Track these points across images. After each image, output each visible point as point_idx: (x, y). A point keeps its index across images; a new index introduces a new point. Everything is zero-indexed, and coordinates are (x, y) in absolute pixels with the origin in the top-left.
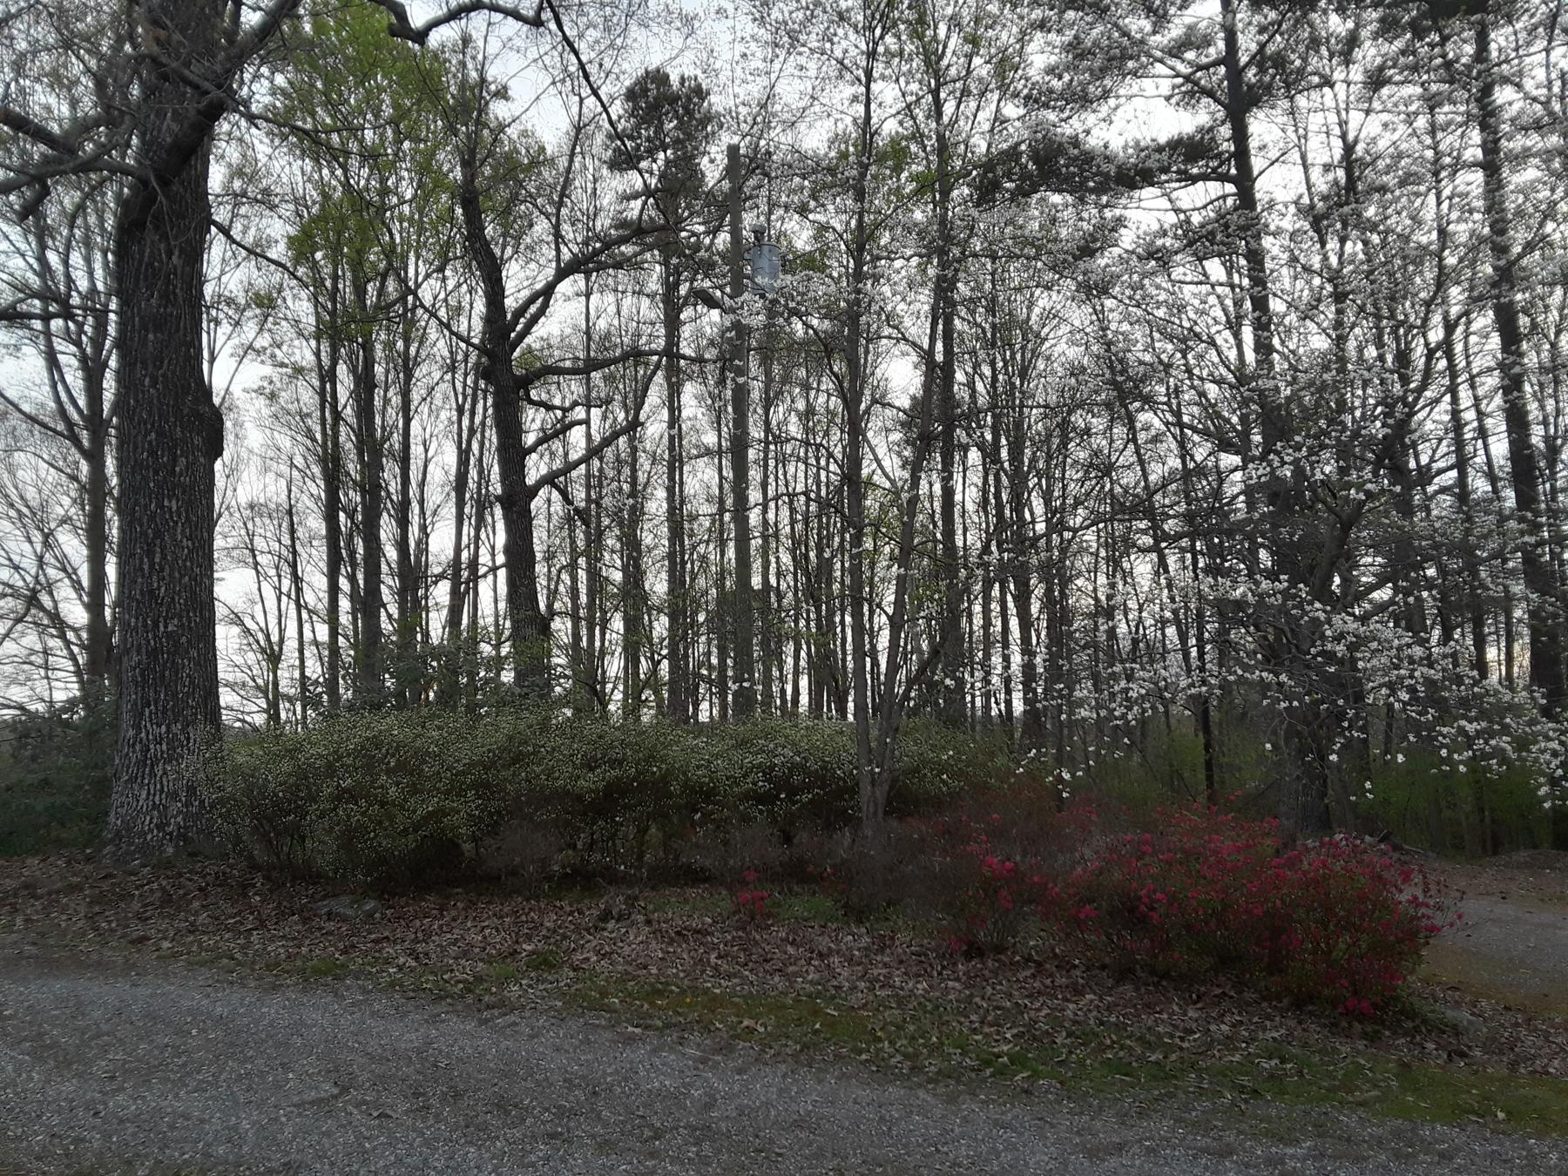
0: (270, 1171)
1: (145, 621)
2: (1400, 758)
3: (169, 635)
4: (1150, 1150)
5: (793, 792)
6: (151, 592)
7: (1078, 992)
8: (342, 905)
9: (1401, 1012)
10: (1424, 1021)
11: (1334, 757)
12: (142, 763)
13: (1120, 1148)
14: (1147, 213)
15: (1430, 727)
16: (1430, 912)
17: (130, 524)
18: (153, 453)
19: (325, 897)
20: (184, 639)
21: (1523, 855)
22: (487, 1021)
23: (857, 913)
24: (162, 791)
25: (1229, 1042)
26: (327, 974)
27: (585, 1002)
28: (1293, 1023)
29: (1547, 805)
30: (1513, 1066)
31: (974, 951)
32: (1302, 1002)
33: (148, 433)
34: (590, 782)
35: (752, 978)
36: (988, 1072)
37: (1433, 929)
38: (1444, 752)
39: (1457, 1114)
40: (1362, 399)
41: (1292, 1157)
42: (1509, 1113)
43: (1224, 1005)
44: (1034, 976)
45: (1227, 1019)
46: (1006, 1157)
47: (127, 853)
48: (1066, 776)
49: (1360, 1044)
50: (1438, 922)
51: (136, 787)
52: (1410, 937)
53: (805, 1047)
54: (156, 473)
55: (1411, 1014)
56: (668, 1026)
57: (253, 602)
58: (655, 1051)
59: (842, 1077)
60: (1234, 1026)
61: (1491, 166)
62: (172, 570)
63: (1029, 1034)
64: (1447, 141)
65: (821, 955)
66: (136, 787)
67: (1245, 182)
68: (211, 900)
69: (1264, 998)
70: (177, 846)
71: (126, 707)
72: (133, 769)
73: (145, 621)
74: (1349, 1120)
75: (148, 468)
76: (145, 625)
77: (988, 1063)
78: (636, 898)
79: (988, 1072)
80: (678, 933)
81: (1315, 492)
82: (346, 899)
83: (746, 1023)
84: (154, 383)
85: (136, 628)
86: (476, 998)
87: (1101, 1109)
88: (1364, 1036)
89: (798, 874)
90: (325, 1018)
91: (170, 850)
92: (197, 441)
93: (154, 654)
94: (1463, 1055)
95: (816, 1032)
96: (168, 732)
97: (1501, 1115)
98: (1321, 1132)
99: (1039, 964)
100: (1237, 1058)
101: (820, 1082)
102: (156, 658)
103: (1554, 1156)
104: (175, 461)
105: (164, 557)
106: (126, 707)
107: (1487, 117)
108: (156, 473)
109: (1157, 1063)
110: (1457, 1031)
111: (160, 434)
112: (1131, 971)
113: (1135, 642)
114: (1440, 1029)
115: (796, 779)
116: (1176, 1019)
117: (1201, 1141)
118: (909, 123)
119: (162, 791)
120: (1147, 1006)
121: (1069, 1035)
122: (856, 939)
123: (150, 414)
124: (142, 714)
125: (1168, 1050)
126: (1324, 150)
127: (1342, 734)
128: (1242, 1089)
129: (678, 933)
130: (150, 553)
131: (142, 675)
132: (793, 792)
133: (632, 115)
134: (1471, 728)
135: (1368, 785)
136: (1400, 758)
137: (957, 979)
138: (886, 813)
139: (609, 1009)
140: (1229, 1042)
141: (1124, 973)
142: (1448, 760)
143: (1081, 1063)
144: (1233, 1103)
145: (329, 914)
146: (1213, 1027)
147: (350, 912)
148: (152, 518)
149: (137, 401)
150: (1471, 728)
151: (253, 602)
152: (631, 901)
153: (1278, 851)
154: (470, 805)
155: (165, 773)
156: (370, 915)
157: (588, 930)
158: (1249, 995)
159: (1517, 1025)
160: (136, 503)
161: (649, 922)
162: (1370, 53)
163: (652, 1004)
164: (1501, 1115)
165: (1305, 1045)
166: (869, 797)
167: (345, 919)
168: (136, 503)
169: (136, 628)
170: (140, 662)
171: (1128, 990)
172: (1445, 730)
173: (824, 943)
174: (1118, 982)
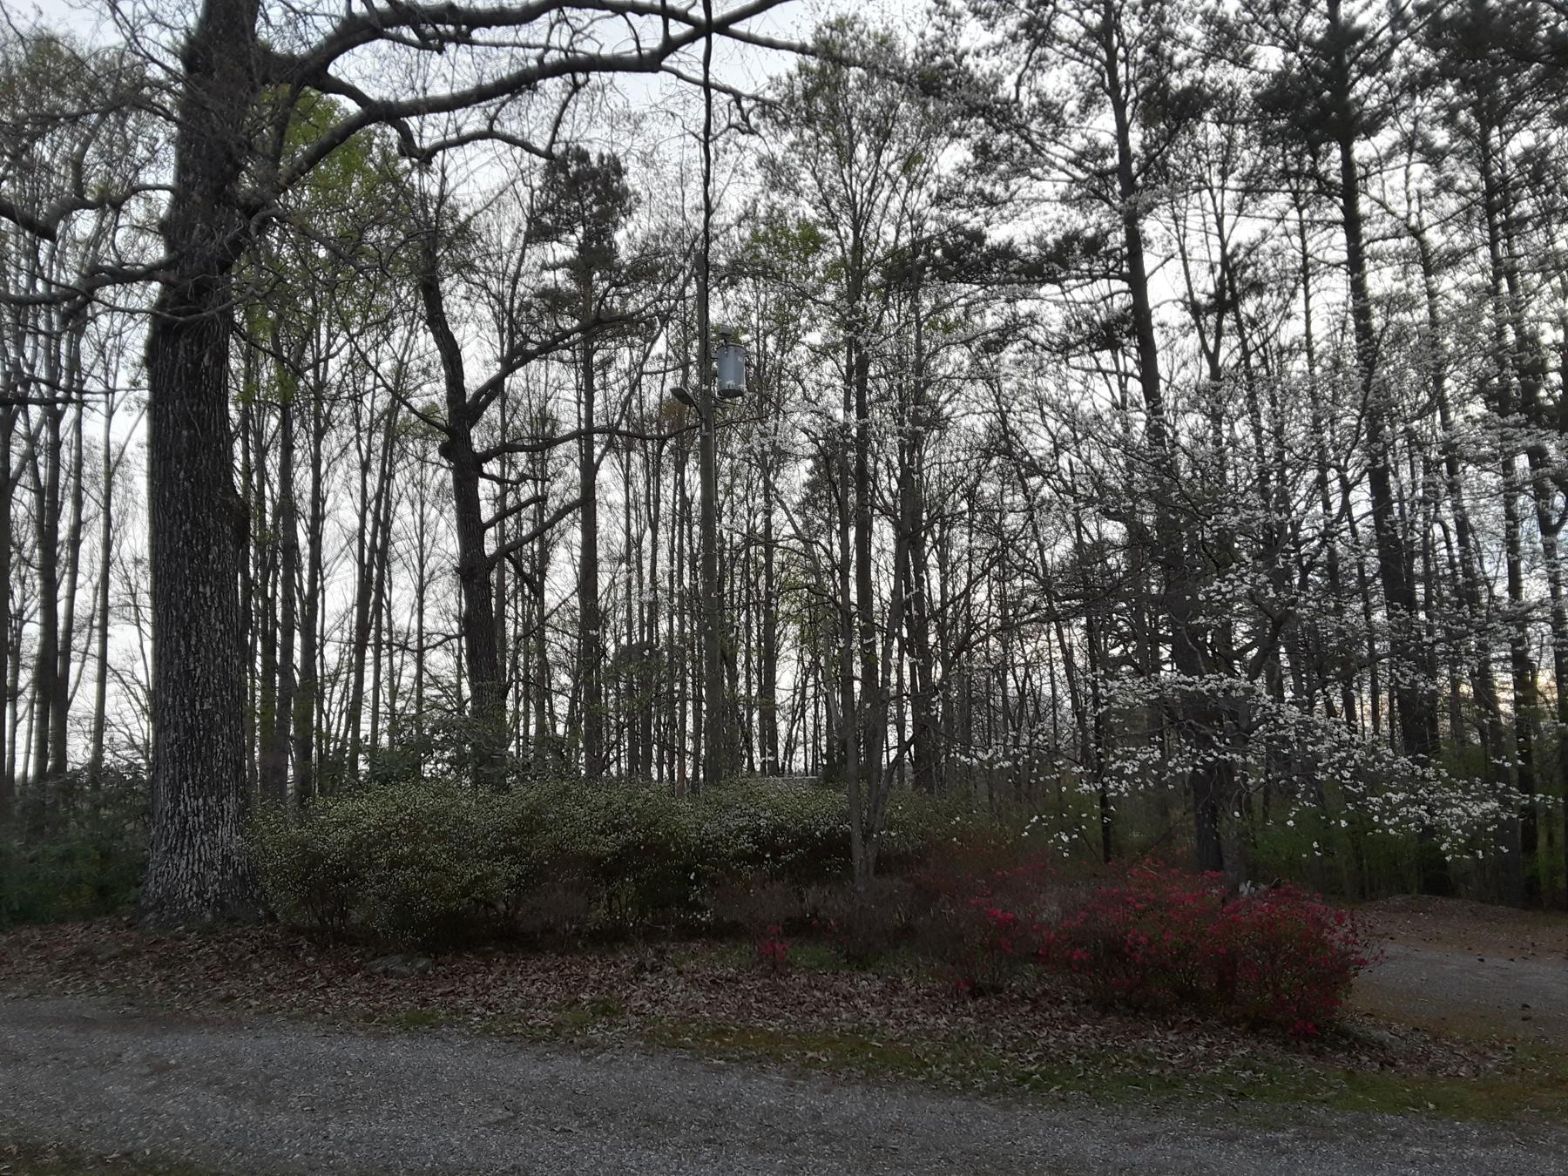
0: (504, 1172)
1: (182, 700)
2: (1343, 823)
3: (205, 713)
4: (1175, 1139)
5: (777, 852)
6: (188, 672)
7: (1075, 1024)
8: (395, 962)
9: (1336, 1032)
10: (1357, 1039)
11: (1290, 823)
12: (181, 834)
13: (1152, 1138)
14: (1051, 308)
15: (1363, 796)
16: (1356, 948)
17: (167, 608)
18: (188, 543)
19: (375, 957)
20: (218, 717)
21: (1398, 900)
22: (590, 1057)
23: (859, 961)
24: (200, 860)
25: (1208, 1059)
26: (418, 1024)
27: (658, 1041)
28: (1254, 1043)
29: (1448, 859)
30: (1432, 1071)
31: (976, 992)
32: (1256, 1025)
33: (183, 523)
34: (607, 845)
35: (794, 1018)
36: (1027, 1086)
37: (1363, 963)
38: (1376, 818)
39: (1399, 1107)
40: (1240, 474)
41: (1284, 1139)
42: (1437, 1104)
43: (1196, 1030)
44: (1032, 1011)
45: (1201, 1041)
46: (1067, 1147)
47: (170, 919)
48: (1066, 839)
49: (1310, 1058)
50: (1365, 955)
51: (175, 857)
52: (1337, 973)
53: (868, 1071)
54: (191, 561)
55: (1345, 1034)
56: (745, 1058)
57: (133, 659)
58: (745, 1078)
59: (909, 1094)
60: (1207, 1046)
61: (1355, 263)
62: (207, 651)
63: (1045, 1056)
64: (1316, 239)
65: (845, 997)
66: (175, 857)
67: (1137, 283)
68: (266, 961)
69: (1225, 1024)
70: (214, 913)
71: (162, 783)
72: (172, 841)
73: (182, 700)
74: (1319, 1113)
75: (183, 556)
76: (182, 704)
77: (1025, 1081)
78: (664, 952)
79: (1027, 1086)
80: (713, 982)
81: (1178, 544)
82: (398, 958)
83: (810, 1054)
84: (187, 479)
85: (174, 706)
86: (556, 1038)
87: (1127, 1112)
88: (1311, 1051)
89: (803, 928)
90: (446, 1056)
91: (209, 916)
92: (228, 530)
93: (190, 731)
94: (1392, 1065)
95: (871, 1060)
96: (205, 804)
97: (1431, 1106)
98: (1299, 1122)
99: (1034, 1001)
100: (1219, 1070)
101: (895, 1097)
102: (193, 735)
103: (1475, 1132)
104: (208, 550)
105: (199, 640)
106: (162, 783)
107: (1352, 223)
108: (191, 561)
109: (1157, 1076)
110: (1382, 1046)
111: (195, 524)
112: (1112, 1005)
113: (1022, 693)
114: (1367, 1044)
115: (780, 840)
116: (1156, 1041)
117: (1215, 1131)
118: (823, 210)
119: (200, 860)
120: (1133, 1032)
121: (1079, 1057)
122: (869, 984)
123: (186, 505)
124: (180, 787)
125: (1163, 1066)
126: (1203, 251)
127: (1296, 804)
128: (1230, 1093)
129: (713, 982)
130: (187, 637)
131: (181, 752)
132: (777, 852)
133: (552, 188)
134: (1396, 798)
135: (1315, 845)
136: (1343, 823)
137: (969, 1015)
138: (876, 872)
139: (685, 1046)
140: (1208, 1059)
141: (1106, 1008)
142: (1380, 825)
143: (1098, 1077)
144: (1227, 1103)
145: (385, 972)
146: (1192, 1048)
147: (404, 970)
148: (188, 603)
149: (172, 493)
150: (1396, 798)
151: (133, 659)
152: (660, 953)
153: (1223, 901)
154: (508, 870)
155: (203, 843)
156: (424, 971)
157: (630, 981)
158: (1213, 1022)
159: (1426, 1042)
160: (172, 588)
161: (680, 973)
162: (1248, 159)
163: (721, 1041)
164: (1431, 1106)
165: (1267, 1060)
166: (861, 855)
167: (402, 976)
168: (172, 588)
169: (174, 706)
170: (177, 739)
171: (1112, 1019)
172: (1374, 800)
173: (844, 986)
174: (1103, 1015)
